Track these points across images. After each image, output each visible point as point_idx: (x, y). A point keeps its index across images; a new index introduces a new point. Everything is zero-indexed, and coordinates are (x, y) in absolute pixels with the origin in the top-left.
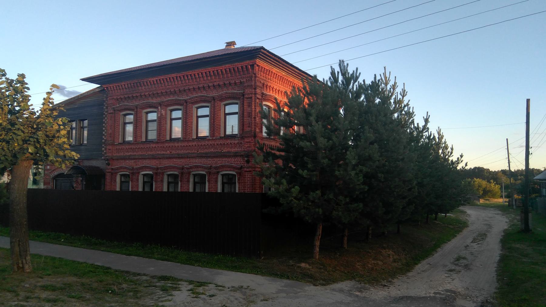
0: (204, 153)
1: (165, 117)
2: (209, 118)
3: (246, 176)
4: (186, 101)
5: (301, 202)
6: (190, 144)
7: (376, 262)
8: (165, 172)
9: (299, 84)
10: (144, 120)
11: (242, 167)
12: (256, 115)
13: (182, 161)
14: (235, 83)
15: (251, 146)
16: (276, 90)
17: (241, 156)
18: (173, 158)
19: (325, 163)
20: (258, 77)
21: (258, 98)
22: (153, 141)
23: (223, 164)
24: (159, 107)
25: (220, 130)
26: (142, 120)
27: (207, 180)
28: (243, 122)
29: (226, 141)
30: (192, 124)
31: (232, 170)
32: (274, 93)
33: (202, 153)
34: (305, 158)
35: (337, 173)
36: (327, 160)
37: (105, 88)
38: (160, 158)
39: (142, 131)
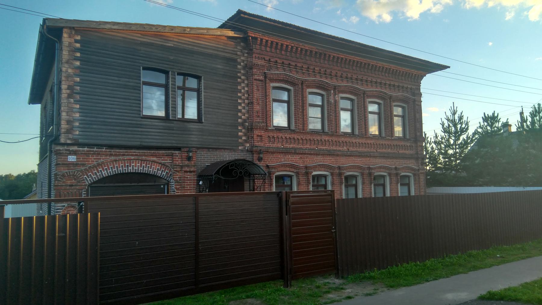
6: (369, 141)
31: (325, 170)
38: (338, 155)
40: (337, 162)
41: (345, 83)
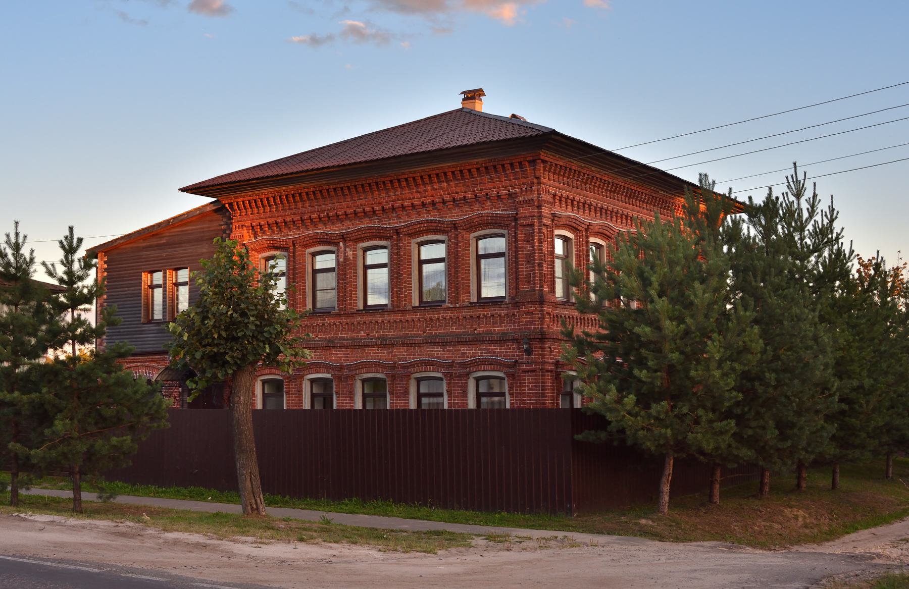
0: (437, 336)
1: (354, 263)
2: (387, 269)
3: (525, 380)
4: (397, 231)
5: (639, 418)
6: (408, 317)
7: (768, 524)
8: (357, 374)
9: (625, 185)
10: (310, 270)
11: (516, 362)
12: (542, 260)
13: (392, 353)
14: (499, 197)
15: (535, 321)
16: (578, 203)
17: (516, 341)
18: (372, 346)
19: (674, 358)
20: (544, 184)
21: (544, 225)
22: (330, 312)
23: (476, 356)
24: (341, 244)
25: (469, 290)
26: (305, 269)
27: (388, 389)
28: (516, 272)
29: (482, 311)
30: (411, 278)
32: (575, 210)
33: (433, 336)
34: (643, 351)
35: (693, 373)
36: (677, 353)
37: (227, 206)
38: (346, 347)
39: (305, 292)
40: (347, 357)
41: (367, 224)
